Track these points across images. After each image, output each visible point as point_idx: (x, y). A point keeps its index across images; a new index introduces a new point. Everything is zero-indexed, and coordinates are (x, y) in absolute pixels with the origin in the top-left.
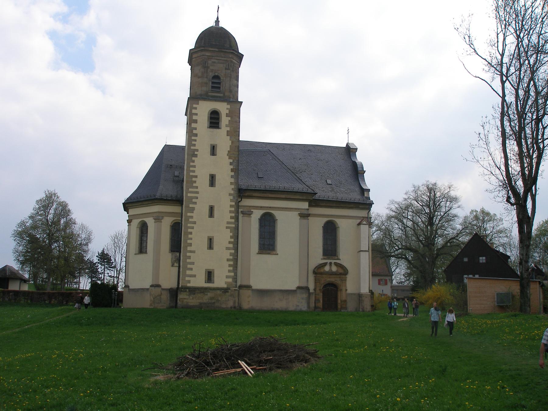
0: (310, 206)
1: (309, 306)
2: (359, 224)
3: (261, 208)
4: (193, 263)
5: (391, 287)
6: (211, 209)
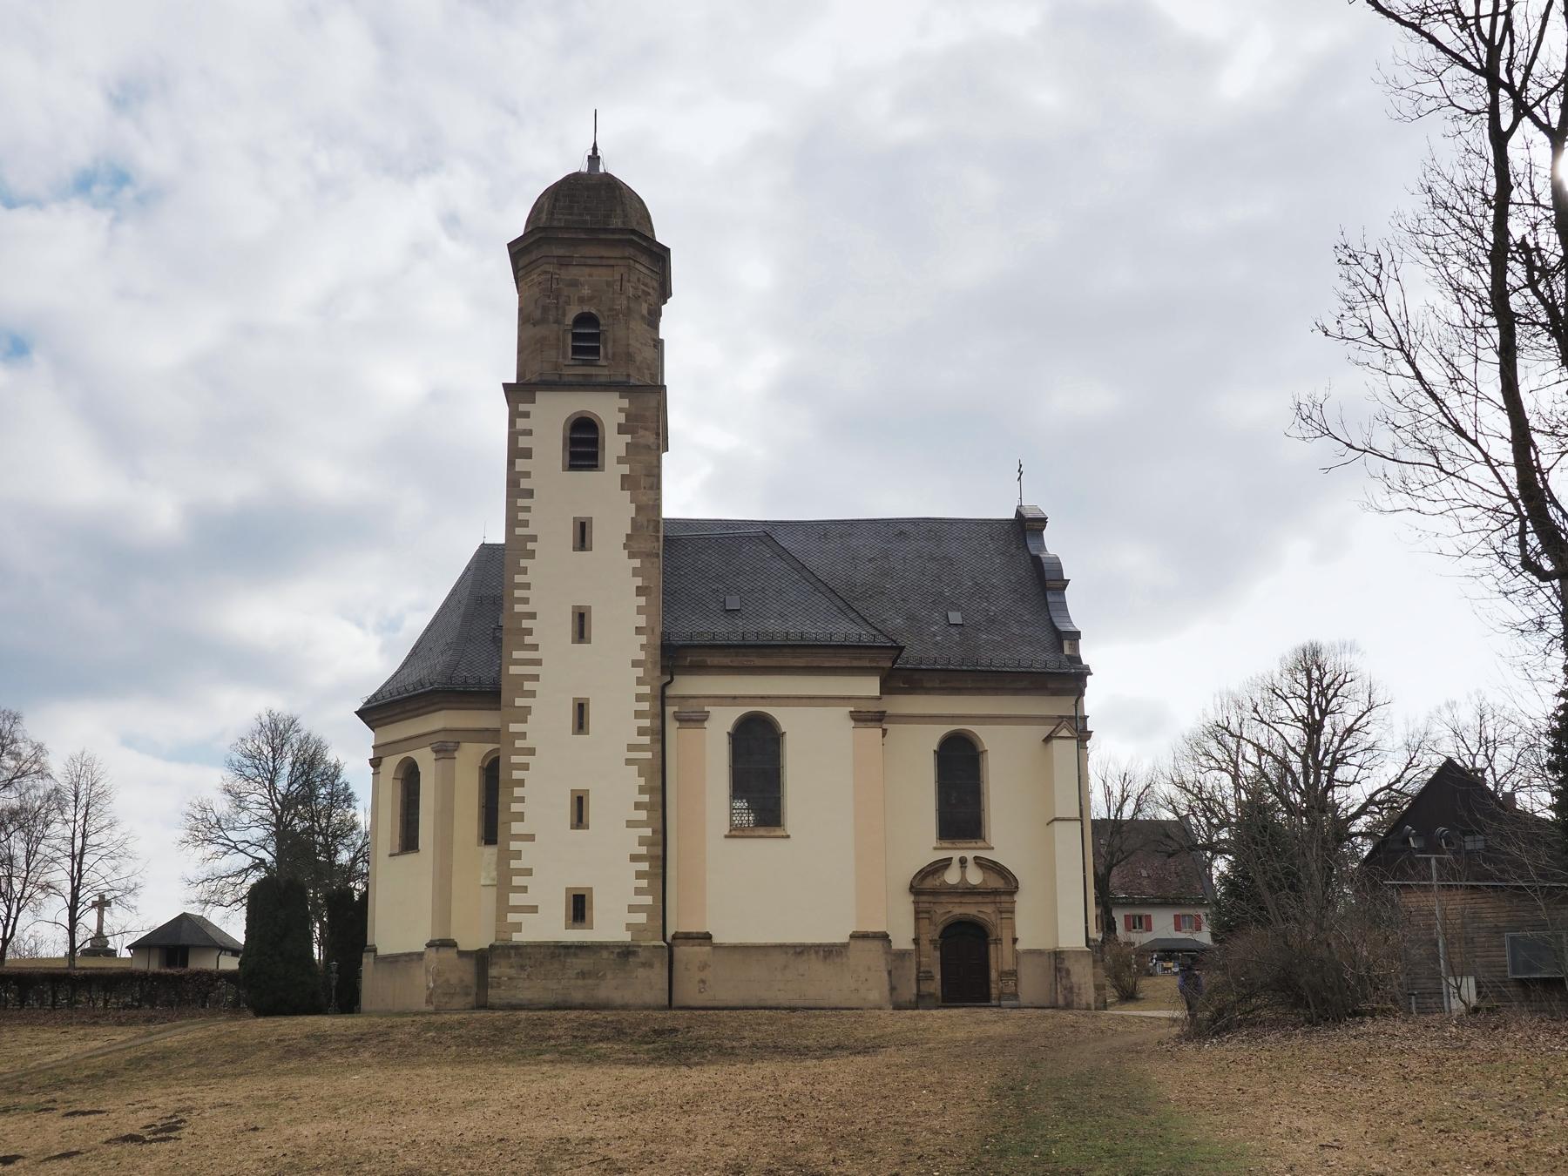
0: (886, 689)
2: (1048, 739)
3: (734, 700)
4: (528, 872)
6: (581, 709)
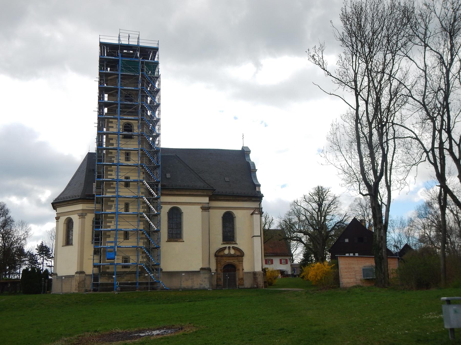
0: (210, 200)
1: (211, 284)
2: (252, 214)
3: (169, 203)
5: (291, 265)
